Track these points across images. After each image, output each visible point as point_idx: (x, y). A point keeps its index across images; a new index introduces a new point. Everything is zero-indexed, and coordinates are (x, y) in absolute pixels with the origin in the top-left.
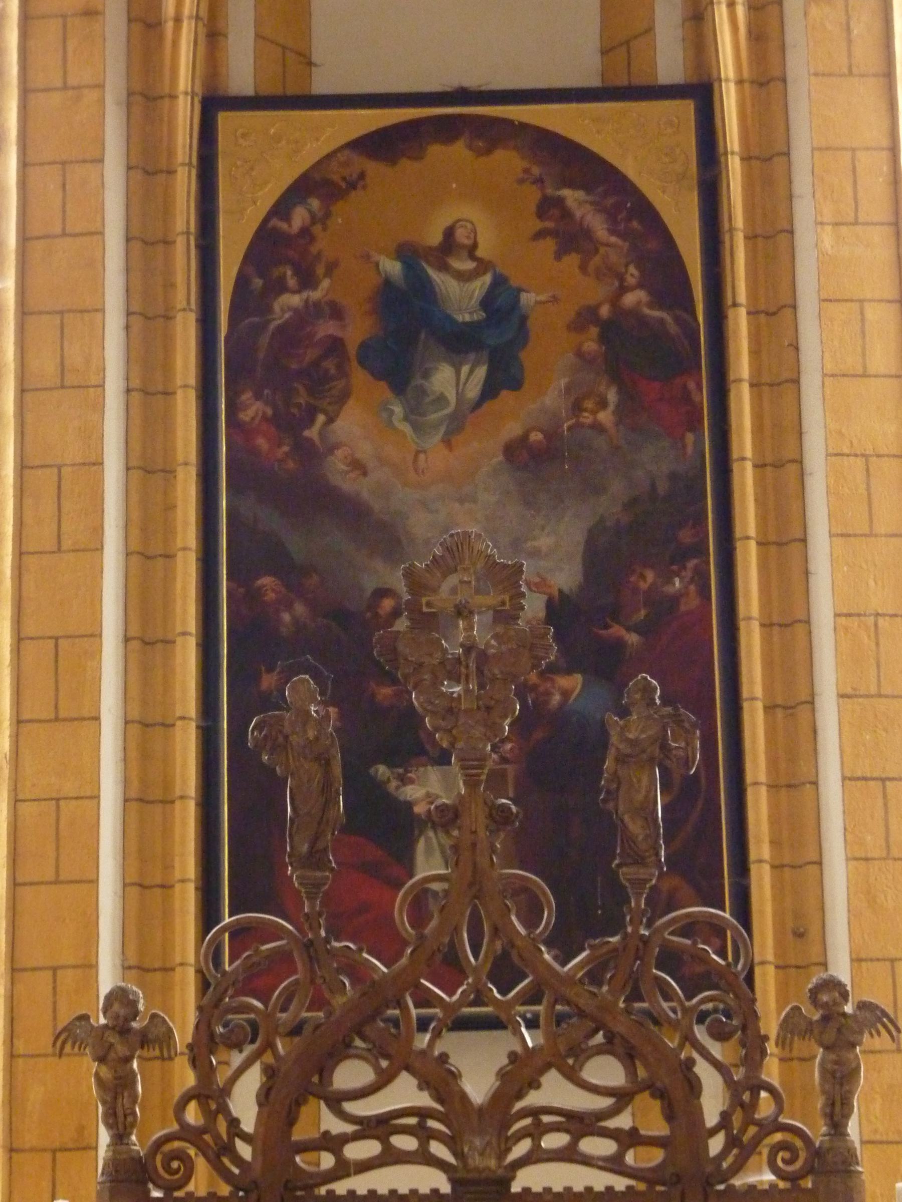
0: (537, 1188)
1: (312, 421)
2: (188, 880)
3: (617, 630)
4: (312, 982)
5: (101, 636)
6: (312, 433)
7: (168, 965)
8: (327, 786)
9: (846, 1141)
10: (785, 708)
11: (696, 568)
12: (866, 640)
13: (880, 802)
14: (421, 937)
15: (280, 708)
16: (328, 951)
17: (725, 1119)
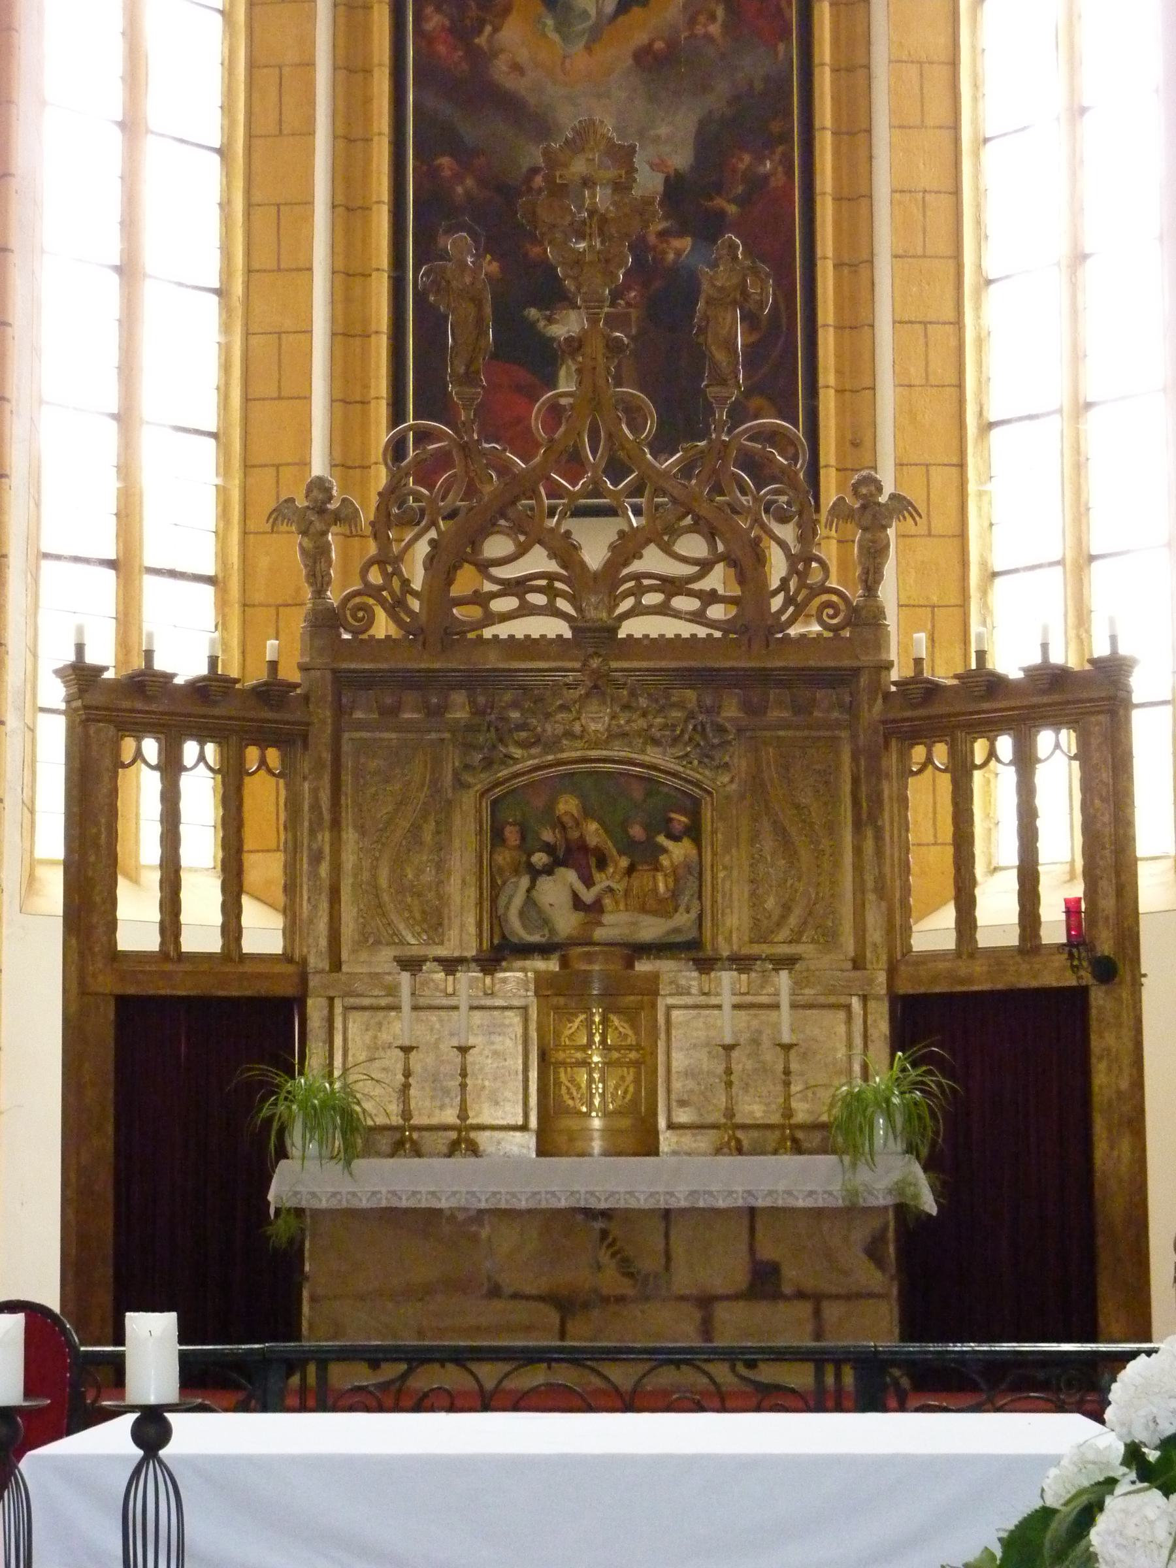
0: (638, 635)
1: (480, 32)
2: (382, 398)
3: (719, 202)
4: (467, 473)
5: (313, 203)
6: (481, 40)
7: (365, 464)
8: (480, 321)
9: (877, 601)
10: (850, 266)
11: (783, 154)
12: (915, 211)
13: (922, 340)
14: (551, 440)
15: (442, 258)
16: (479, 451)
17: (785, 582)
